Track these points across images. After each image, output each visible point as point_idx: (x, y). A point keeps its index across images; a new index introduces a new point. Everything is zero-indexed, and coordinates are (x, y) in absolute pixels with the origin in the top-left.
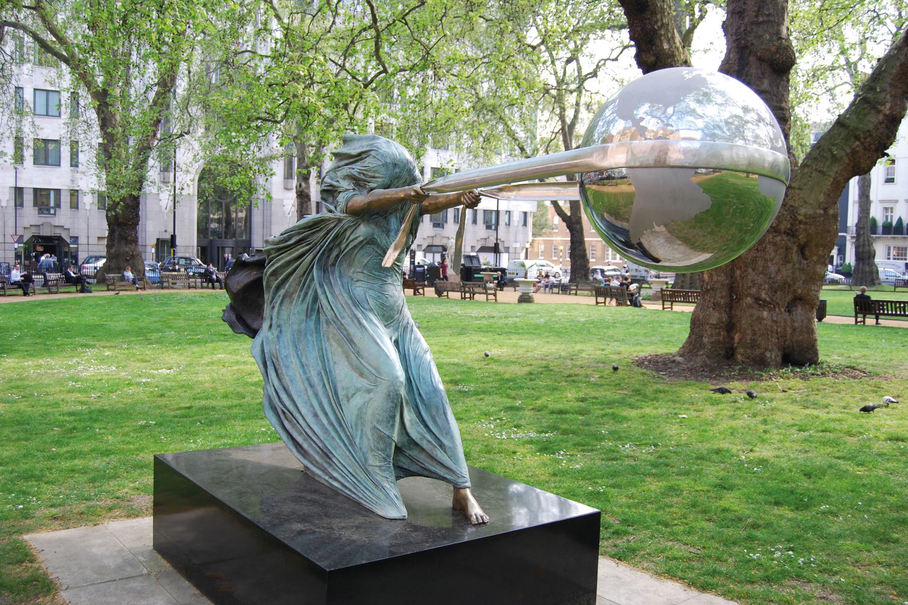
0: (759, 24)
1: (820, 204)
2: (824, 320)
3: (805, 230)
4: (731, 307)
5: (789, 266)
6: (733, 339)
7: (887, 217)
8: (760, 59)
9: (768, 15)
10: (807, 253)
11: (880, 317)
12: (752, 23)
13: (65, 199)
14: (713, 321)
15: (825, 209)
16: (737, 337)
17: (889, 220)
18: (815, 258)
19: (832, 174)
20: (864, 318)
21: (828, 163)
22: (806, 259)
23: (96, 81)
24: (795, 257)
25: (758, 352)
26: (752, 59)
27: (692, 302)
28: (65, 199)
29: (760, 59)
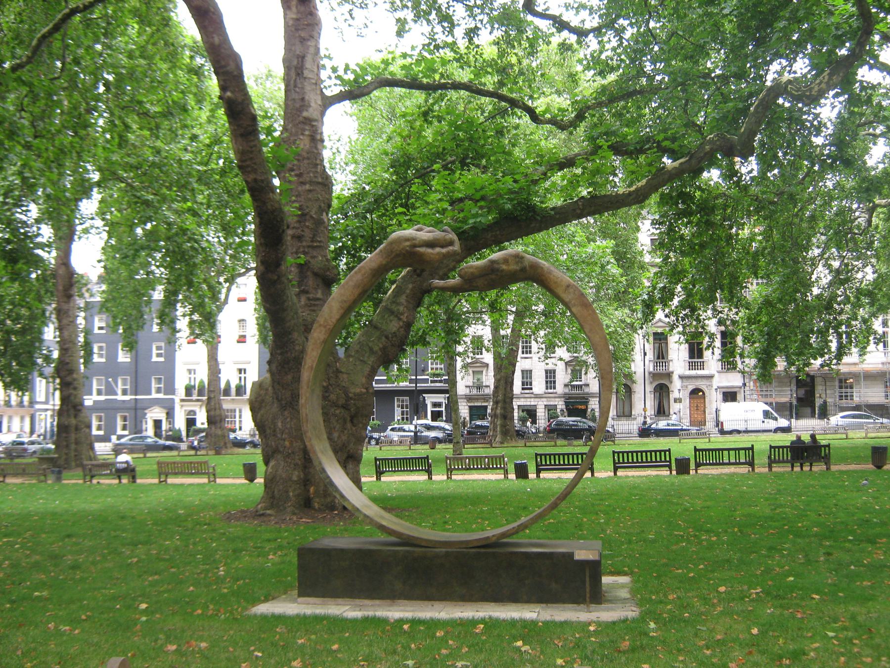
0: (314, 247)
1: (363, 385)
2: (885, 467)
3: (355, 404)
4: (305, 467)
5: (346, 432)
6: (309, 491)
7: (240, 378)
8: (316, 275)
9: (320, 242)
10: (355, 421)
11: (774, 465)
12: (309, 247)
13: (73, 429)
14: (295, 478)
15: (367, 389)
16: (312, 490)
17: (243, 383)
18: (361, 425)
19: (370, 363)
20: (811, 465)
21: (367, 355)
22: (354, 426)
23: (56, 258)
24: (349, 425)
25: (329, 499)
26: (309, 273)
27: (497, 468)
28: (73, 429)
29: (316, 275)
